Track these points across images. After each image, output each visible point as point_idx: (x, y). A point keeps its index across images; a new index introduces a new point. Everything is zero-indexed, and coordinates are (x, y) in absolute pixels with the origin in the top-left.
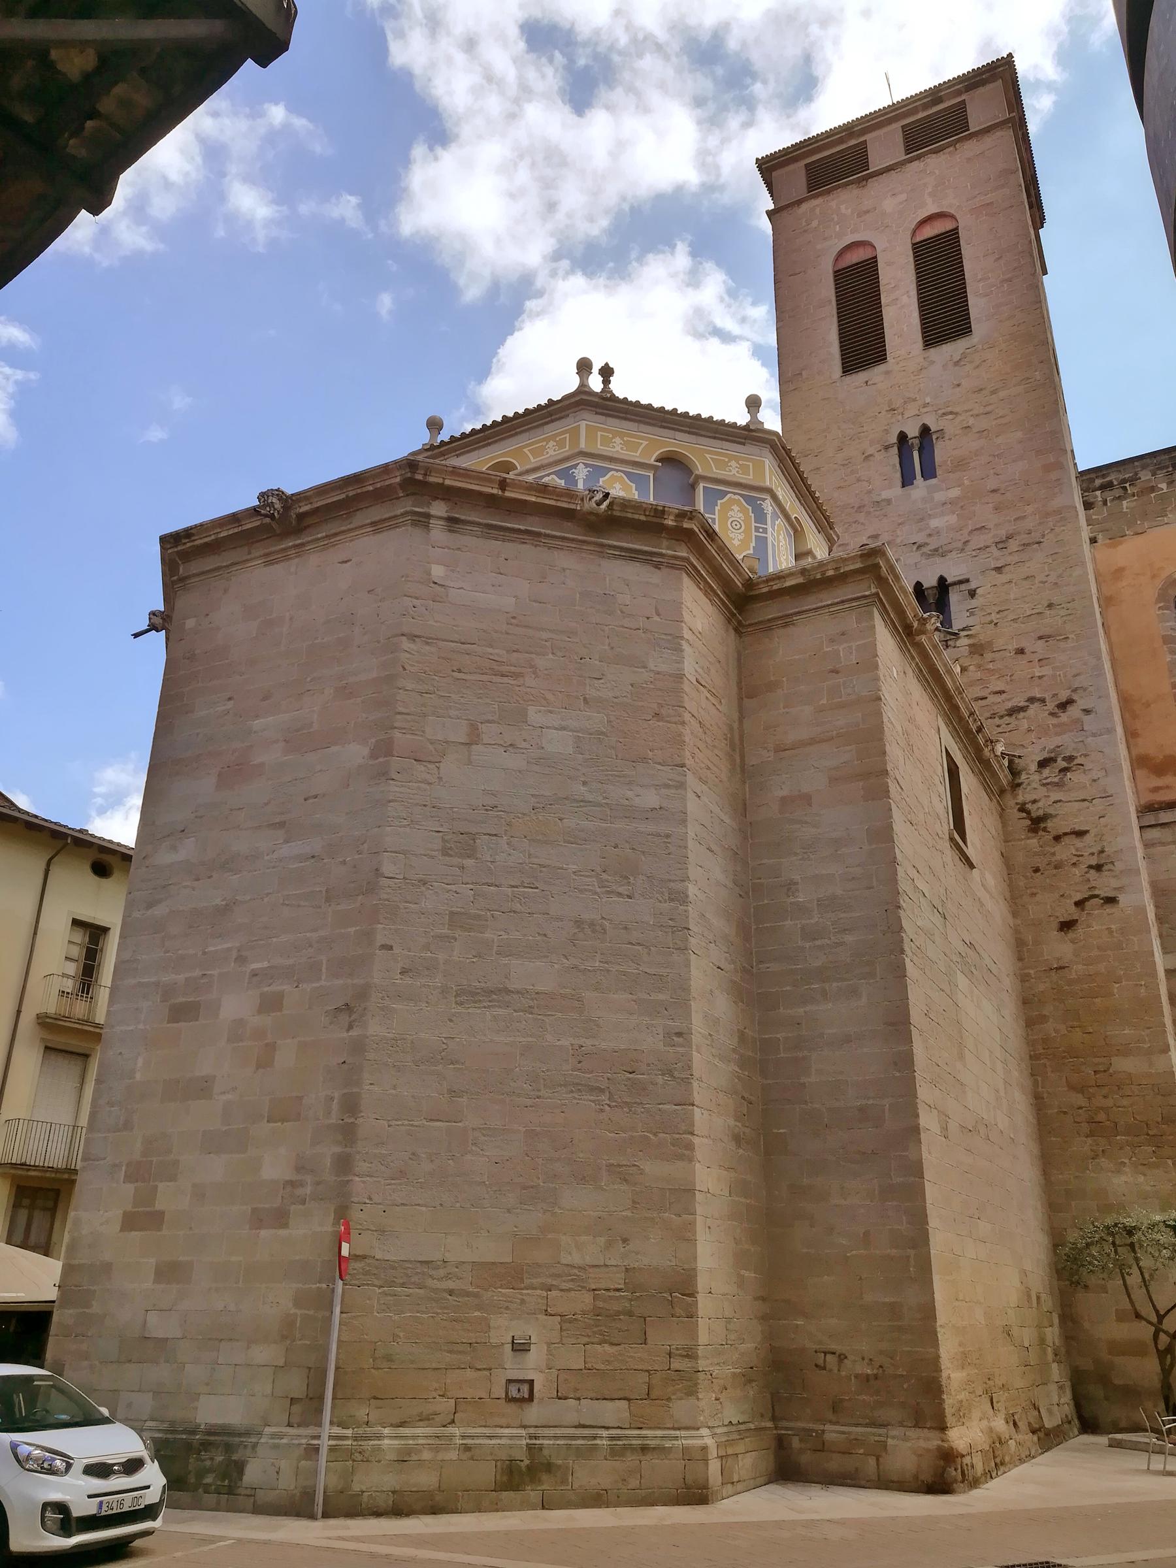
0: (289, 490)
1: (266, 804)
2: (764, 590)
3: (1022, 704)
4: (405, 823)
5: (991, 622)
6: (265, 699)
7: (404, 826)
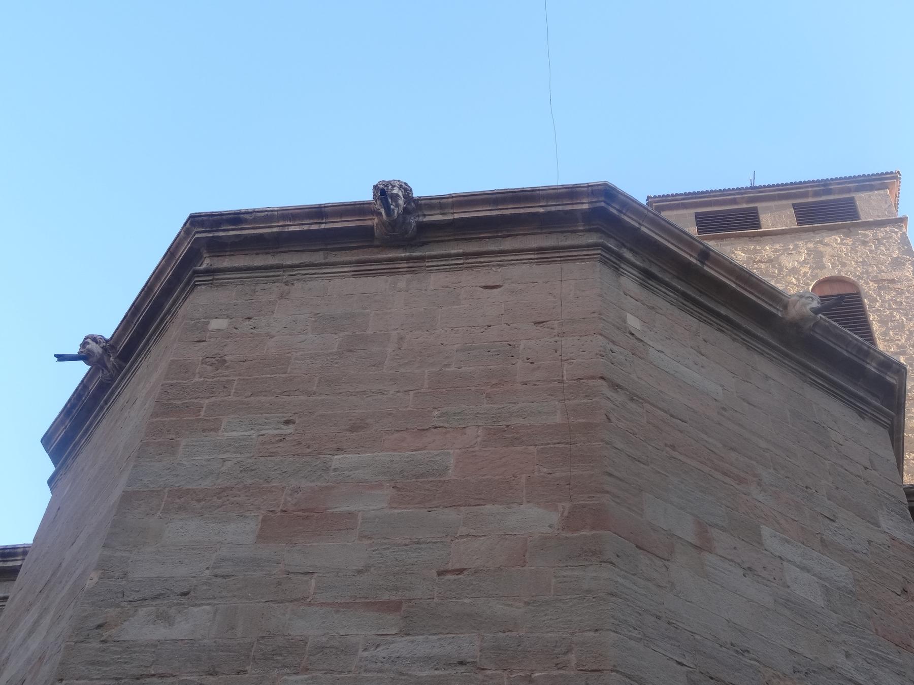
0: (419, 191)
1: (360, 572)
4: (635, 634)
6: (354, 429)
7: (631, 638)
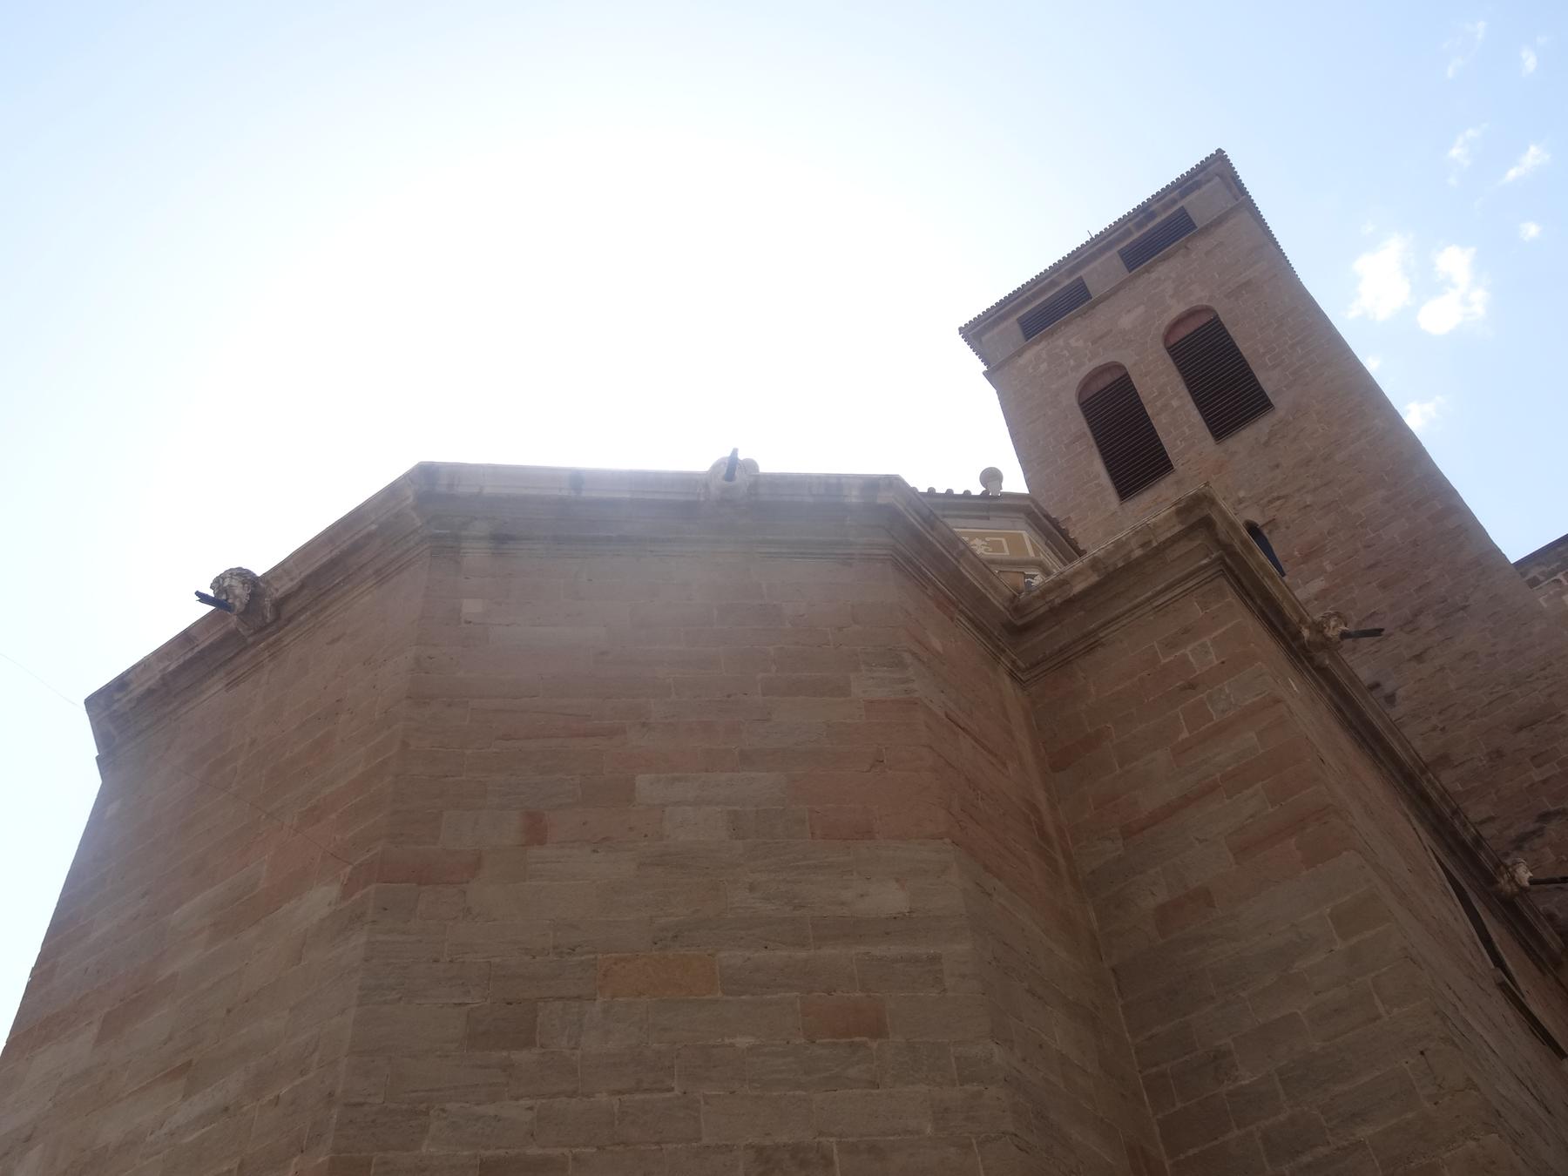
2: (1041, 611)
3: (1531, 827)
5: (1434, 729)
